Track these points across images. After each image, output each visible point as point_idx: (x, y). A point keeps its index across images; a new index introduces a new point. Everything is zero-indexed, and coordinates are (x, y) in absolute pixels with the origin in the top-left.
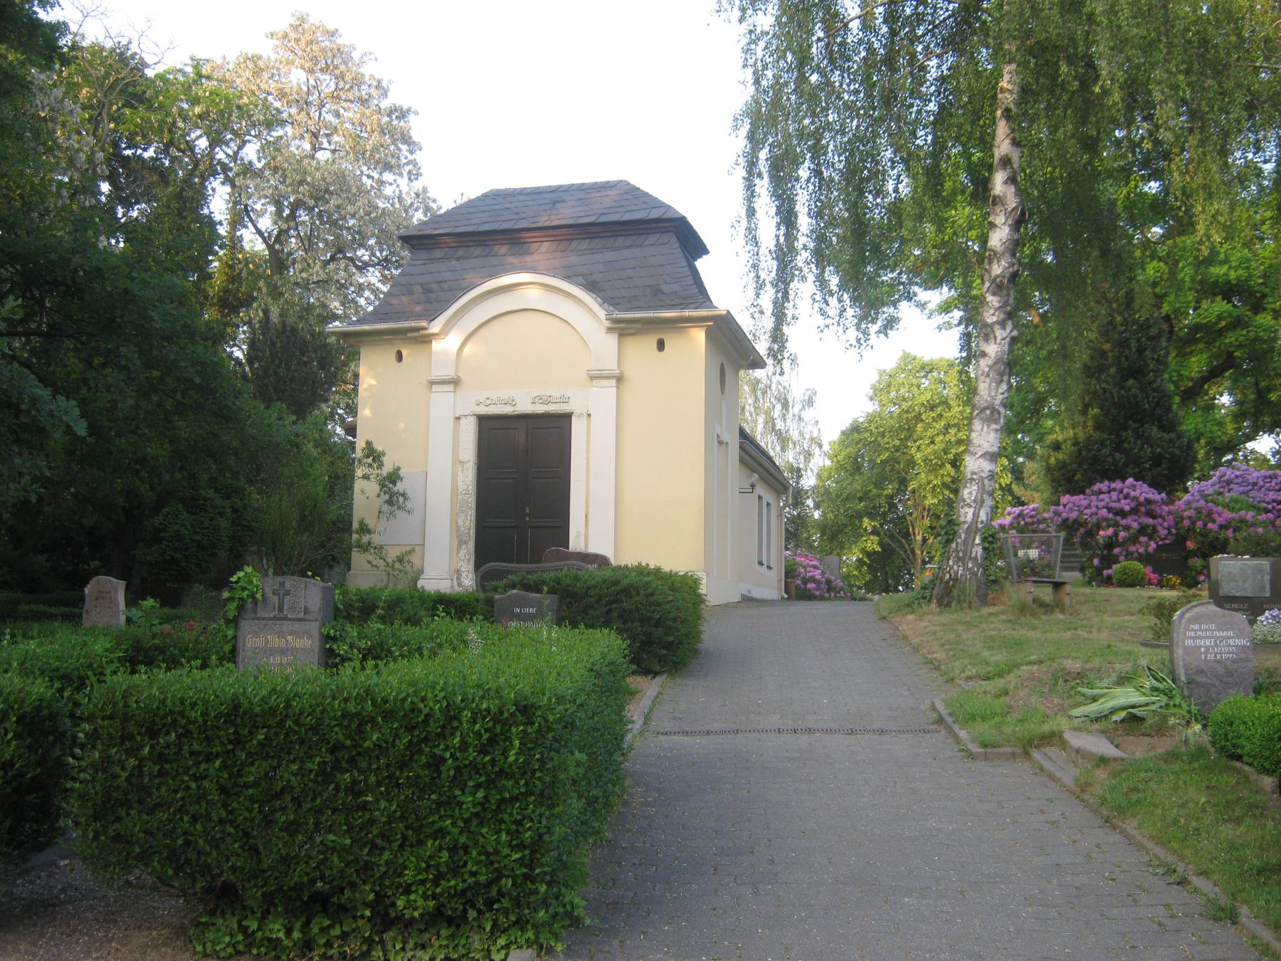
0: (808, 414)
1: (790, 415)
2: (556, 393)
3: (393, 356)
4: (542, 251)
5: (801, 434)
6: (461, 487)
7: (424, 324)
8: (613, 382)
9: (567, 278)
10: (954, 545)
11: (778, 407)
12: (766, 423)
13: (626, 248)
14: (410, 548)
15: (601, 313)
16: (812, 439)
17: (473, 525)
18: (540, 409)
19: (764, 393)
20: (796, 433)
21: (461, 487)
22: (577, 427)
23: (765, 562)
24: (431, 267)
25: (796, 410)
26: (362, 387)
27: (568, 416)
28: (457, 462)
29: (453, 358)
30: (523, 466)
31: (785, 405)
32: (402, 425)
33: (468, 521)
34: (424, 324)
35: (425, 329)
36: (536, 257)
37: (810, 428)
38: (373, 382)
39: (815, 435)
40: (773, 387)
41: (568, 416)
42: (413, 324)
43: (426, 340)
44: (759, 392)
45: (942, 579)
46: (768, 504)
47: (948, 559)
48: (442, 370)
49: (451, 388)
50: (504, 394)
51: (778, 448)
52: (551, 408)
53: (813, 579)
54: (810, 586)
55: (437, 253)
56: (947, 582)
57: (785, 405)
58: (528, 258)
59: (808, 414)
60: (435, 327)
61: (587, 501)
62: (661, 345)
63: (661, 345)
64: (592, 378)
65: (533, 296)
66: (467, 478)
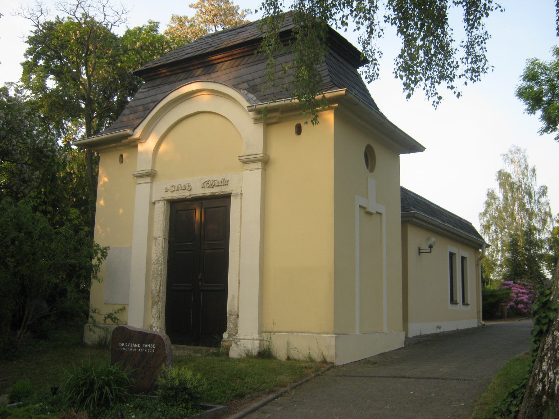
0: (543, 200)
1: (533, 200)
2: (218, 177)
3: (293, 129)
4: (225, 69)
5: (540, 210)
6: (154, 257)
7: (129, 131)
8: (259, 165)
9: (235, 86)
10: (549, 340)
11: (527, 197)
12: (519, 206)
13: (282, 55)
14: (121, 307)
15: (246, 104)
16: (546, 213)
17: (164, 289)
18: (208, 192)
19: (518, 189)
20: (537, 210)
21: (154, 257)
22: (234, 204)
23: (459, 297)
24: (152, 92)
25: (537, 197)
26: (100, 183)
27: (227, 197)
28: (151, 238)
29: (150, 155)
30: (197, 238)
31: (530, 197)
32: (121, 211)
33: (159, 285)
34: (129, 131)
35: (131, 135)
36: (219, 74)
37: (545, 207)
38: (106, 179)
39: (547, 210)
40: (523, 186)
41: (227, 197)
42: (120, 133)
43: (134, 145)
44: (515, 190)
45: (532, 389)
46: (463, 259)
47: (541, 361)
48: (144, 166)
49: (148, 180)
50: (183, 182)
51: (527, 219)
52: (216, 190)
53: (522, 302)
54: (521, 306)
55: (158, 82)
56: (539, 397)
57: (530, 197)
58: (213, 75)
59: (543, 200)
60: (138, 134)
61: (239, 264)
62: (299, 130)
63: (299, 130)
64: (245, 162)
65: (204, 101)
66: (159, 251)
